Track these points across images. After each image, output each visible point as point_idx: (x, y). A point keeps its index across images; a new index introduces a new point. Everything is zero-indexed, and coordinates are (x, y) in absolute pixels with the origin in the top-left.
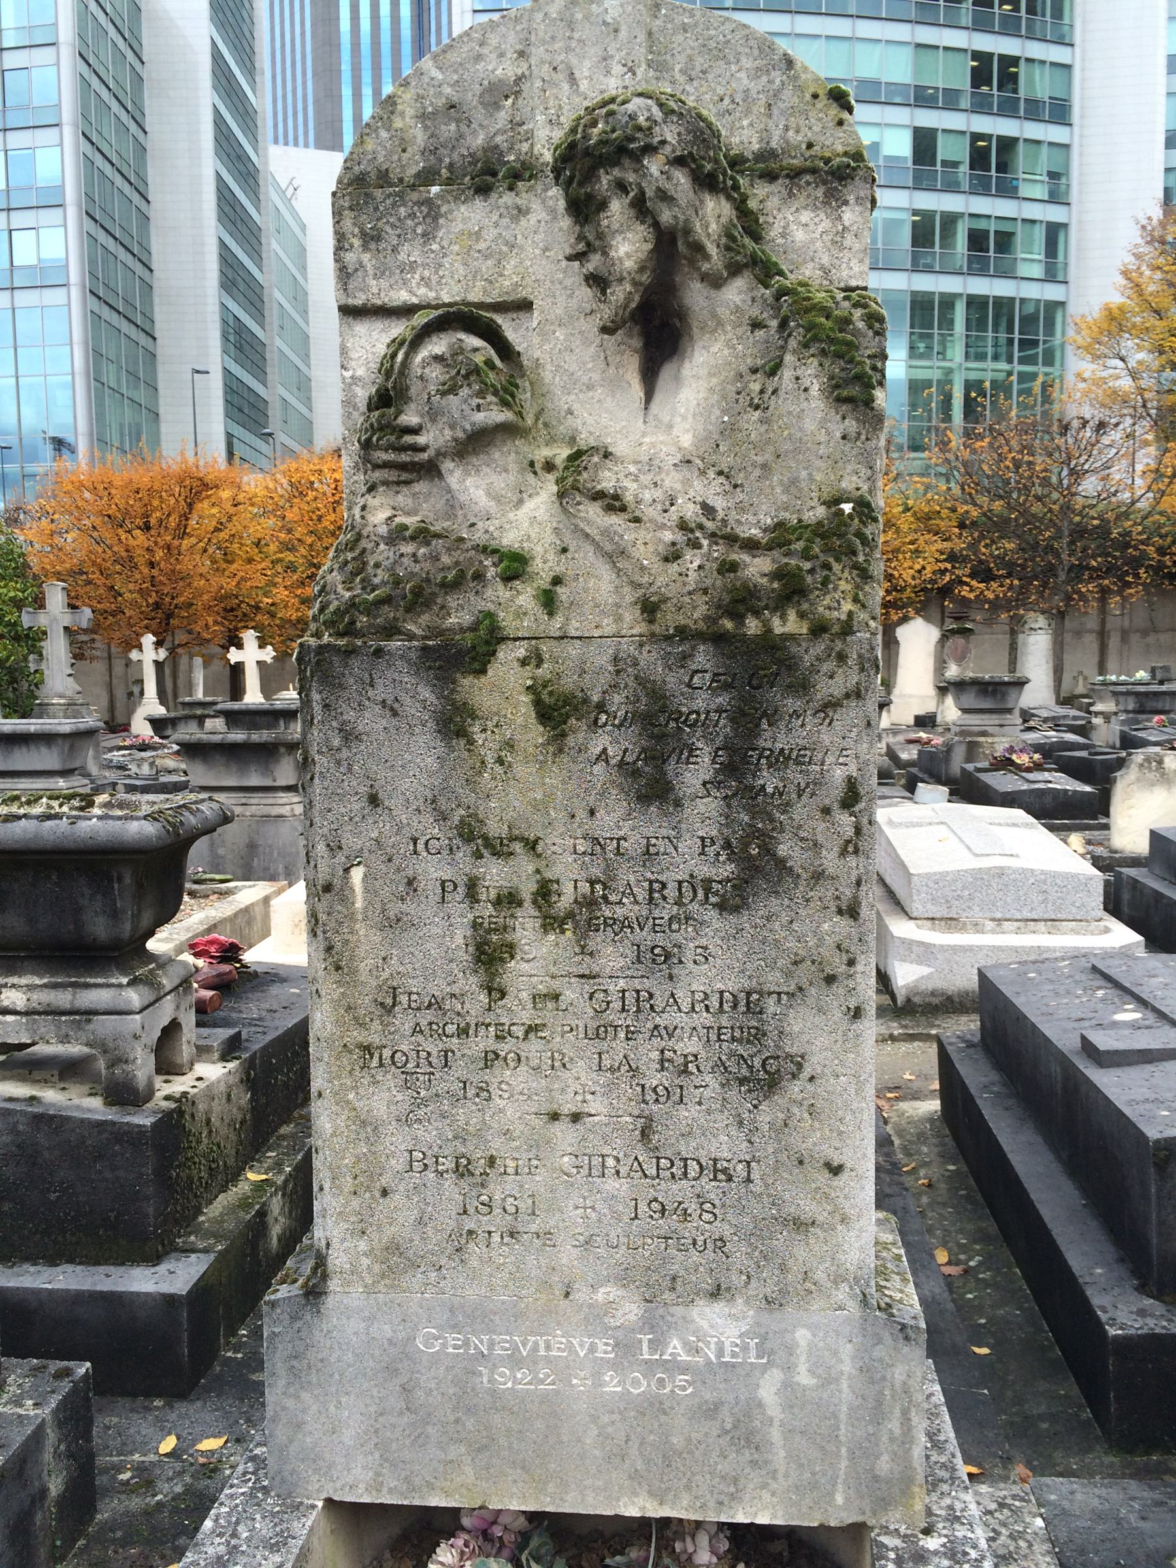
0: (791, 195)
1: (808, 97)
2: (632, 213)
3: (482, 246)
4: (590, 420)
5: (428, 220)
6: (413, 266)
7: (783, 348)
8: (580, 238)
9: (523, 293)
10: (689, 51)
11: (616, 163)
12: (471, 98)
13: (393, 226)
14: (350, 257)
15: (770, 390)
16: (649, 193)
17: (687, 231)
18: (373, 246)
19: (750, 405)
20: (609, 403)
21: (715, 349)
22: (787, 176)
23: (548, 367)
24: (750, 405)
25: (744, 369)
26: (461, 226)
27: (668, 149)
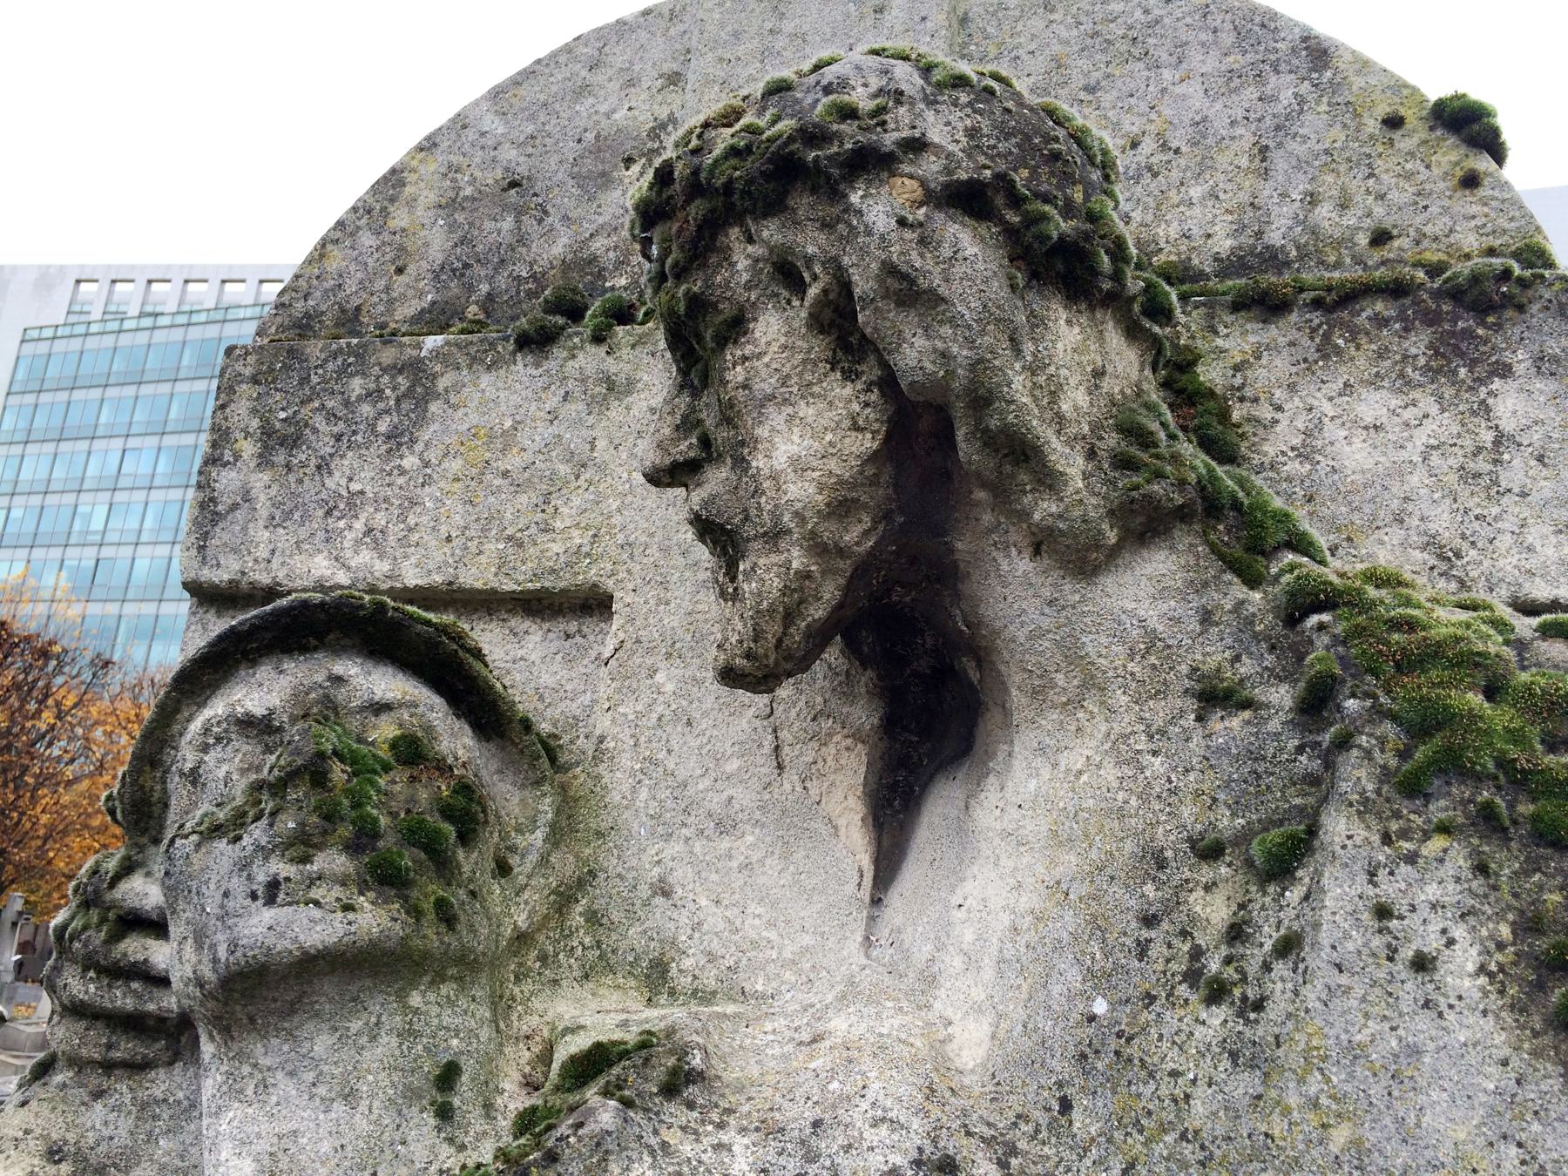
0: (1326, 350)
1: (1372, 125)
2: (819, 346)
3: (513, 462)
4: (714, 919)
5: (406, 405)
6: (354, 502)
7: (1320, 784)
8: (688, 424)
9: (591, 574)
10: (1057, 48)
11: (774, 206)
12: (553, 170)
13: (332, 416)
14: (227, 481)
15: (1268, 937)
16: (862, 285)
17: (982, 399)
18: (280, 457)
19: (1192, 976)
20: (771, 874)
21: (1074, 759)
22: (1317, 304)
23: (626, 761)
24: (1192, 976)
25: (1167, 837)
26: (474, 418)
27: (930, 166)
